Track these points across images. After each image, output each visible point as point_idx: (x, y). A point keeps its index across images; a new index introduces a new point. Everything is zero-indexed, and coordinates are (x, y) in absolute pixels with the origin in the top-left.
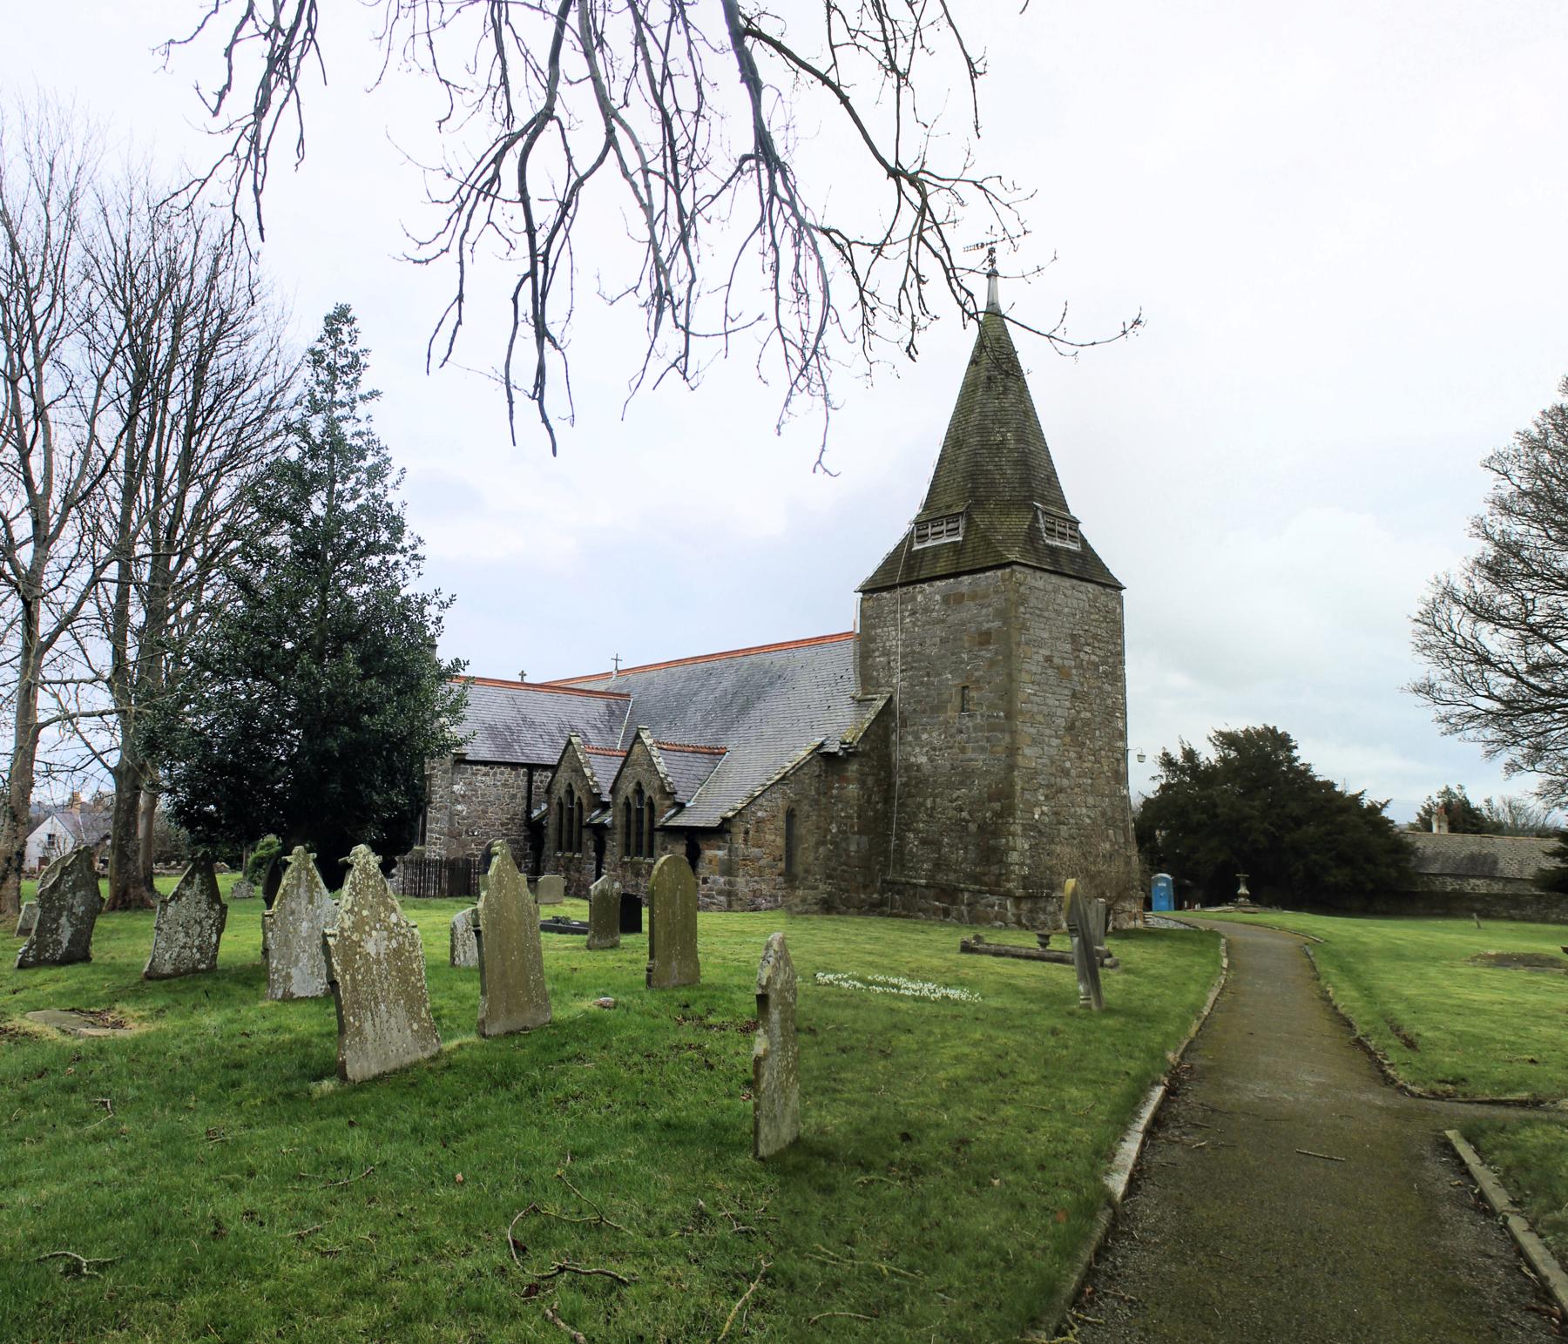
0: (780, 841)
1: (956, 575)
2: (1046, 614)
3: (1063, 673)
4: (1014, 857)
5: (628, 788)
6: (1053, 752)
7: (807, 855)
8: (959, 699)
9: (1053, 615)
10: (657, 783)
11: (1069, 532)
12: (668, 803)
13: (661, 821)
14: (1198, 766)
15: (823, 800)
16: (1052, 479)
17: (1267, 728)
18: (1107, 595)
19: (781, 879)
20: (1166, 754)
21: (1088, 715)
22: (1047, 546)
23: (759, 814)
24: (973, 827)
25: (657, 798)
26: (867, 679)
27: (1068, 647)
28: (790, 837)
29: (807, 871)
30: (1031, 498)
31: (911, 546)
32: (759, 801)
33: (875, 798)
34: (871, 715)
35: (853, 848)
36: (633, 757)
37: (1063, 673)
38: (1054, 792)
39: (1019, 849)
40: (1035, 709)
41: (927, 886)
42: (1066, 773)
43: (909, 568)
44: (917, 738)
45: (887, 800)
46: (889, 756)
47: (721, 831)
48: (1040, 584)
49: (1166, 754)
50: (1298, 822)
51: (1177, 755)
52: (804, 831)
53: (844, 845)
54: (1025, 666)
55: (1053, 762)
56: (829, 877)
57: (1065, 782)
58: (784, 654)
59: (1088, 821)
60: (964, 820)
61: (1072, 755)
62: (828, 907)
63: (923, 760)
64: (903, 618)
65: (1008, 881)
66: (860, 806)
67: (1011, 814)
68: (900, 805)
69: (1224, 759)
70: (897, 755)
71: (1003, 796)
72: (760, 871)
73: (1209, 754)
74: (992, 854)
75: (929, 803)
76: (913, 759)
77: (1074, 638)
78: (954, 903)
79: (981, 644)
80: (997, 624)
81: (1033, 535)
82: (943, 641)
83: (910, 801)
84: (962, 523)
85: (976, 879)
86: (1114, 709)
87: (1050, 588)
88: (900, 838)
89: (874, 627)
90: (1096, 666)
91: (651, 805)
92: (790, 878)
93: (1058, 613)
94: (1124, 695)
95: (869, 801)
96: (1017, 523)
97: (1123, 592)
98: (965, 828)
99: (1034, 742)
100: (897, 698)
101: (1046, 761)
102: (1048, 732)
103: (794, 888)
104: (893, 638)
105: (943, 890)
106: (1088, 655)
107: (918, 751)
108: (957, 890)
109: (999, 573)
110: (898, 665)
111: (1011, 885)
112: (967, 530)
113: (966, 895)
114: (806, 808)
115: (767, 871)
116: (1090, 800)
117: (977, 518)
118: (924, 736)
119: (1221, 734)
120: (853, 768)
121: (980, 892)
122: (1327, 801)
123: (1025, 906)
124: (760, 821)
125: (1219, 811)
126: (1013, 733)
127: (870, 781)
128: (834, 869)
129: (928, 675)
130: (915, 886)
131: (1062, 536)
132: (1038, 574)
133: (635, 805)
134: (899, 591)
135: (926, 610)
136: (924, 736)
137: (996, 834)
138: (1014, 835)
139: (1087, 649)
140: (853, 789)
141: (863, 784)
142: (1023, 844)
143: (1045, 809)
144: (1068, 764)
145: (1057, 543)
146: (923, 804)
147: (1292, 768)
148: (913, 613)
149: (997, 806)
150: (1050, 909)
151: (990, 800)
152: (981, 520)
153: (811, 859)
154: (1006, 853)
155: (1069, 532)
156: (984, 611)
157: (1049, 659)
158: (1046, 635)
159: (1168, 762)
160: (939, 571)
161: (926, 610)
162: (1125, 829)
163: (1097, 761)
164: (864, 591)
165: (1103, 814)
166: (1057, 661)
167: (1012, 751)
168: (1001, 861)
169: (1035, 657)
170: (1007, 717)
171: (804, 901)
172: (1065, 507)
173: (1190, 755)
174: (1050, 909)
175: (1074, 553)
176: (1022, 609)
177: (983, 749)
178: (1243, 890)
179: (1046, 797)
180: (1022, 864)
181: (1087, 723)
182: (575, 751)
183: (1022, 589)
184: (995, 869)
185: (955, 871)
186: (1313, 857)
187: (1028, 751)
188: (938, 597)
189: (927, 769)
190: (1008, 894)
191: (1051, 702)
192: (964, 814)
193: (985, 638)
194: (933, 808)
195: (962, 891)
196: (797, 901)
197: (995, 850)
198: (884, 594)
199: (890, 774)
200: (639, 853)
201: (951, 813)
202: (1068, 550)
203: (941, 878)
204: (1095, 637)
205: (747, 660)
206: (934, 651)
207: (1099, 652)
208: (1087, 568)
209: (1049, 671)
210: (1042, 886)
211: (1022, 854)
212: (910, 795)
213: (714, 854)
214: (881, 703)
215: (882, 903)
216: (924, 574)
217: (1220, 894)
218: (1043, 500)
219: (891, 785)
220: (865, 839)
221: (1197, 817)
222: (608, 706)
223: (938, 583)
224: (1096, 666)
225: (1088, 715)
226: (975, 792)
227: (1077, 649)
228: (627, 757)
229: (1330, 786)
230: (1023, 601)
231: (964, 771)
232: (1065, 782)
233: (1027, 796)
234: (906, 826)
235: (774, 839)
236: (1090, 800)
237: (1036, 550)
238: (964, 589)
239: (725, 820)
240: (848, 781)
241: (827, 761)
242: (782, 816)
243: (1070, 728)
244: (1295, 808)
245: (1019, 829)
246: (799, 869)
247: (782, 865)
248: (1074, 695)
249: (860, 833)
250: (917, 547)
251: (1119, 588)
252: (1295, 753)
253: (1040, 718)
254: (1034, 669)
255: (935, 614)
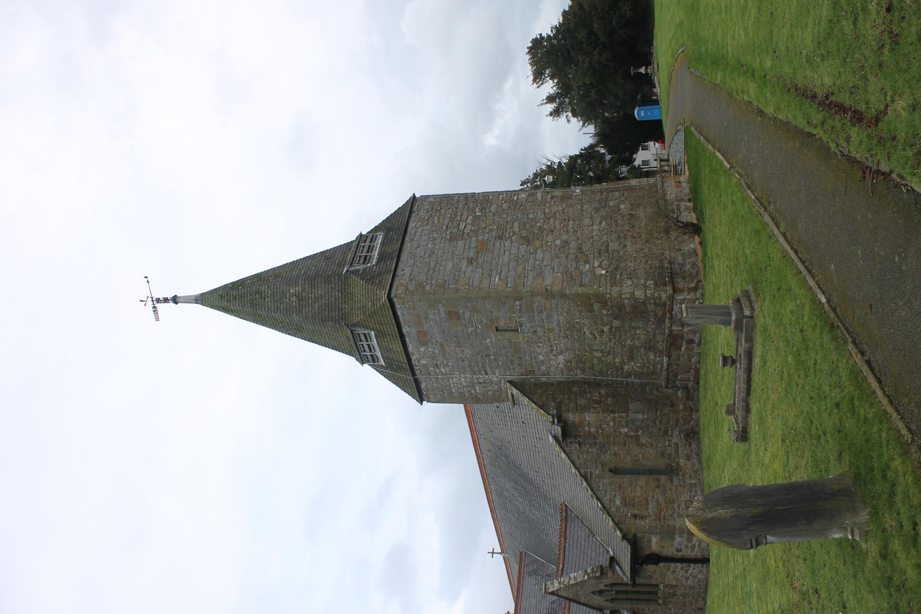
0: (642, 481)
1: (402, 337)
2: (433, 264)
3: (482, 248)
4: (639, 294)
5: (598, 600)
6: (548, 256)
7: (649, 456)
8: (507, 333)
9: (434, 258)
10: (593, 582)
11: (367, 243)
12: (610, 574)
13: (627, 578)
14: (558, 93)
15: (600, 439)
16: (326, 256)
17: (529, 52)
18: (419, 210)
19: (675, 480)
20: (551, 114)
21: (516, 224)
22: (377, 263)
23: (618, 503)
24: (616, 323)
25: (606, 581)
26: (497, 398)
27: (460, 244)
28: (637, 471)
29: (663, 455)
30: (340, 275)
31: (382, 366)
32: (606, 503)
33: (596, 397)
34: (525, 400)
35: (640, 416)
36: (571, 596)
37: (482, 248)
38: (582, 255)
39: (631, 290)
40: (512, 273)
41: (669, 356)
42: (565, 243)
43: (399, 368)
44: (543, 362)
45: (598, 385)
46: (560, 383)
47: (634, 542)
48: (407, 271)
49: (551, 114)
50: (591, 32)
51: (550, 107)
52: (629, 458)
53: (638, 423)
54: (476, 284)
55: (557, 257)
56: (666, 432)
57: (573, 245)
58: (482, 441)
59: (604, 224)
60: (610, 330)
61: (550, 238)
62: (692, 435)
63: (561, 358)
64: (442, 374)
65: (660, 298)
66: (604, 411)
67: (603, 296)
68: (601, 374)
69: (552, 79)
70: (558, 377)
71: (587, 302)
72: (670, 502)
73: (549, 87)
74: (639, 310)
75: (599, 354)
76: (561, 366)
77: (453, 238)
78: (682, 337)
79: (459, 318)
80: (440, 306)
81: (369, 277)
82: (459, 344)
83: (597, 368)
84: (361, 331)
85: (660, 321)
86: (512, 201)
87: (411, 261)
88: (629, 375)
89: (451, 394)
90: (476, 218)
91: (612, 585)
92: (671, 471)
93: (432, 253)
94: (499, 193)
95: (599, 402)
96: (358, 286)
97: (417, 196)
98: (618, 329)
99: (541, 274)
100: (510, 378)
101: (556, 261)
102: (531, 261)
103: (679, 468)
104: (460, 380)
105: (671, 345)
106: (467, 225)
107: (555, 364)
108: (671, 334)
109: (398, 306)
110: (482, 377)
111: (664, 297)
112: (365, 327)
113: (674, 328)
114: (607, 456)
115: (669, 495)
116: (587, 221)
117: (355, 319)
118: (541, 357)
119: (534, 80)
120: (571, 417)
121: (671, 318)
122: (575, 16)
123: (681, 284)
124: (625, 503)
125: (588, 82)
126: (533, 294)
127: (582, 402)
128: (660, 429)
129: (488, 355)
130: (669, 365)
131: (370, 249)
132: (399, 272)
133: (613, 594)
134: (419, 376)
135: (434, 357)
136: (541, 357)
137: (621, 307)
138: (620, 295)
139: (462, 226)
140: (589, 417)
141: (584, 409)
142: (627, 286)
143: (596, 264)
144: (558, 242)
145: (376, 253)
146: (599, 359)
147: (555, 36)
148: (437, 366)
149: (596, 306)
150: (680, 259)
151: (591, 310)
152: (356, 318)
153: (650, 451)
154: (636, 300)
155: (367, 243)
156: (431, 316)
157: (470, 261)
158: (450, 265)
159: (556, 113)
160: (400, 348)
161: (434, 357)
162: (609, 191)
163: (554, 216)
164: (421, 401)
165: (597, 210)
166: (471, 255)
167: (549, 294)
168: (644, 303)
169: (468, 274)
170: (520, 299)
171: (688, 458)
172: (349, 245)
173: (550, 99)
174: (680, 259)
175: (384, 239)
176: (428, 288)
177: (549, 316)
178: (642, 70)
179: (586, 262)
180: (645, 286)
181: (523, 225)
182: (568, 587)
183: (411, 287)
184: (651, 307)
185: (655, 335)
186: (614, 24)
187: (548, 281)
188: (422, 349)
189: (569, 356)
190: (672, 299)
191: (506, 260)
192: (606, 329)
193: (454, 316)
194: (602, 351)
195: (671, 331)
196: (689, 464)
197: (634, 308)
198: (423, 386)
199: (575, 383)
200: (656, 593)
201: (605, 338)
202: (382, 243)
203: (661, 346)
204: (452, 219)
205: (488, 466)
206: (468, 352)
207: (464, 217)
208: (397, 226)
209: (480, 260)
210: (662, 267)
211: (637, 286)
212: (592, 367)
213: (655, 544)
214: (515, 391)
215: (686, 388)
216: (403, 359)
217: (648, 81)
218: (341, 265)
219: (585, 382)
220: (632, 406)
221: (593, 94)
222: (530, 574)
223: (410, 349)
224: (476, 218)
225: (516, 224)
226: (586, 321)
227: (462, 235)
228: (570, 600)
229: (565, 14)
230: (421, 286)
231: (569, 329)
232: (573, 245)
233: (586, 281)
234: (619, 370)
235: (640, 487)
236: (587, 221)
237: (380, 274)
238: (414, 331)
239: (624, 537)
240: (582, 422)
241: (567, 435)
242: (618, 479)
243: (527, 240)
244: (582, 35)
245: (615, 290)
246: (661, 463)
247: (663, 479)
248: (500, 237)
249: (627, 411)
250: (382, 362)
251: (414, 198)
252: (544, 35)
253: (520, 269)
254: (478, 276)
255: (437, 351)
